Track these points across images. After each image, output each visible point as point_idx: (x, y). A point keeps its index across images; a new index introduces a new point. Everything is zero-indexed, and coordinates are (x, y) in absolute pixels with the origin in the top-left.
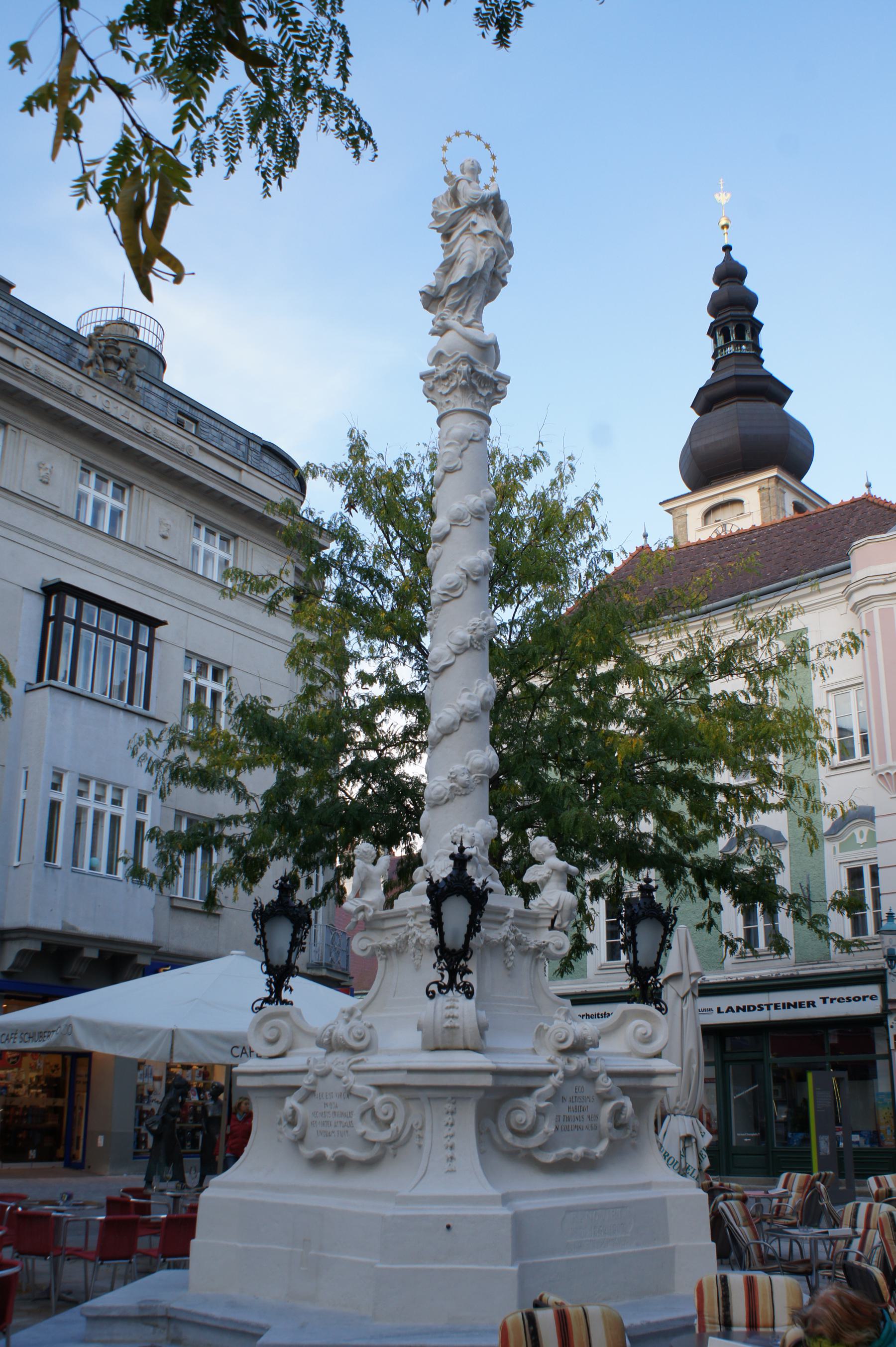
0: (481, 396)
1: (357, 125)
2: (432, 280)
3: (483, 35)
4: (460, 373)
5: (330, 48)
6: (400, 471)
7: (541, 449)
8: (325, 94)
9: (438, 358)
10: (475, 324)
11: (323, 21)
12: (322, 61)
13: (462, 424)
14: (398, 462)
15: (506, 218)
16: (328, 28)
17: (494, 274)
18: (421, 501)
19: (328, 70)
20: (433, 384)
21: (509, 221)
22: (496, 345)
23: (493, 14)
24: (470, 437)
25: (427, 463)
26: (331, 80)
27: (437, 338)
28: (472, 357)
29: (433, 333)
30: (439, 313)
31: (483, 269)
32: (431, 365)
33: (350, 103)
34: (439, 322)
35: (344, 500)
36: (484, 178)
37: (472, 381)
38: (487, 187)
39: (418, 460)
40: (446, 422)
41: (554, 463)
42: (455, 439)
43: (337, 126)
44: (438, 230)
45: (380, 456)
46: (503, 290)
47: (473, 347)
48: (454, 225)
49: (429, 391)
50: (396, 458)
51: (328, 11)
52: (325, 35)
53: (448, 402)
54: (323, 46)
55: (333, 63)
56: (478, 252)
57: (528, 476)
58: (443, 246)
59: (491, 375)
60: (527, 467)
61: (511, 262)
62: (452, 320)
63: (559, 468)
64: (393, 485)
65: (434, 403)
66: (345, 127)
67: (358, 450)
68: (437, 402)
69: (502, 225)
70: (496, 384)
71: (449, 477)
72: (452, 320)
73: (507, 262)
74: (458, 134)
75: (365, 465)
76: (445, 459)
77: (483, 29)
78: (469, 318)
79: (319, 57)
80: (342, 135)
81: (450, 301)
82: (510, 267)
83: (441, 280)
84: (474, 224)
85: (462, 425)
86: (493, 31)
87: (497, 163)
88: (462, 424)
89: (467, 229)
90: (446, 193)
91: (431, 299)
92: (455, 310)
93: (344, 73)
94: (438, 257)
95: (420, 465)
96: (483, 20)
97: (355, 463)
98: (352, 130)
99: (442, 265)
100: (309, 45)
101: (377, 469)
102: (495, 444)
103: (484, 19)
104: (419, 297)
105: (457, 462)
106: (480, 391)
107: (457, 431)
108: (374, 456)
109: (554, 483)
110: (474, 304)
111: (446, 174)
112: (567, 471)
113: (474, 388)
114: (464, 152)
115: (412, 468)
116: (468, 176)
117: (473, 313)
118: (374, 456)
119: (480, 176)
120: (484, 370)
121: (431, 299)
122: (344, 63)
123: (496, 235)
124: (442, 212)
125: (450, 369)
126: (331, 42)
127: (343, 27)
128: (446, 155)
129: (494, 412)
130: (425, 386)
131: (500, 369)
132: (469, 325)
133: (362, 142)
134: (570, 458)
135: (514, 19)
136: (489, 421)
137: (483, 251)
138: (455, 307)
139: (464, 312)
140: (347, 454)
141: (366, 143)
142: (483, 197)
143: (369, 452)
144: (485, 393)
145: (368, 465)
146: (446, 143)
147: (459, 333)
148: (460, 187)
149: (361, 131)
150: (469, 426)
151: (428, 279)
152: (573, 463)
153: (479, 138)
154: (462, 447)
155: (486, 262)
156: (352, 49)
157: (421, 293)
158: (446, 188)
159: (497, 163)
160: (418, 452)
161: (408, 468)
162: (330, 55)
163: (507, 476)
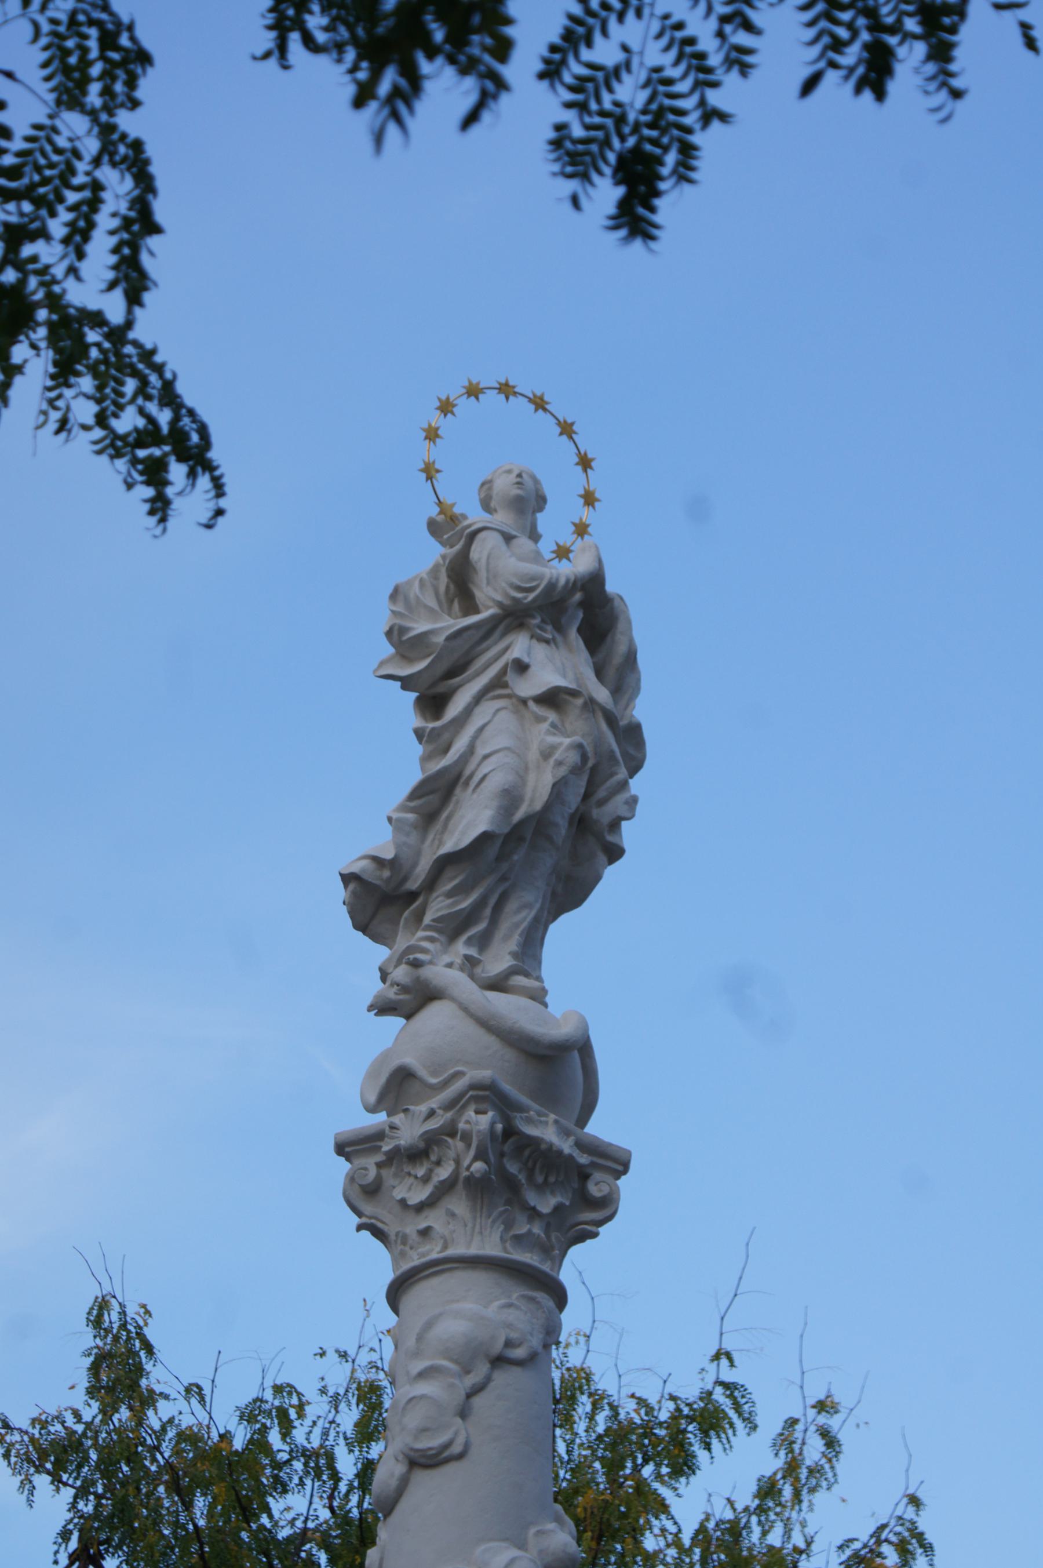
0: (533, 1213)
1: (164, 417)
2: (381, 840)
3: (575, 201)
4: (466, 1138)
5: (94, 204)
6: (259, 1443)
7: (728, 1375)
8: (69, 330)
9: (397, 1086)
10: (519, 980)
11: (74, 125)
12: (66, 241)
13: (469, 1306)
14: (249, 1414)
15: (622, 649)
16: (91, 146)
17: (582, 823)
18: (325, 1544)
19: (84, 267)
20: (378, 1171)
21: (631, 659)
22: (584, 1048)
23: (606, 143)
24: (498, 1347)
25: (349, 1417)
26: (90, 289)
27: (396, 1023)
28: (507, 1087)
29: (383, 1008)
30: (402, 942)
31: (548, 807)
32: (372, 1110)
33: (147, 355)
34: (401, 973)
35: (65, 1535)
36: (555, 526)
37: (507, 1163)
38: (562, 553)
39: (318, 1407)
40: (412, 1299)
41: (770, 1425)
42: (446, 1354)
43: (101, 420)
44: (407, 683)
45: (194, 1391)
46: (612, 874)
47: (510, 1055)
48: (457, 670)
49: (363, 1194)
50: (245, 1398)
51: (94, 96)
52: (81, 167)
53: (425, 1233)
54: (72, 197)
55: (101, 249)
56: (533, 755)
57: (683, 1465)
58: (419, 734)
59: (566, 1147)
60: (681, 1436)
61: (637, 785)
62: (444, 968)
63: (786, 1439)
64: (234, 1489)
65: (379, 1234)
66: (127, 422)
67: (120, 1366)
68: (391, 1230)
69: (611, 672)
70: (584, 1176)
71: (424, 1482)
72: (444, 968)
73: (624, 785)
74: (473, 391)
75: (140, 1420)
76: (414, 1419)
77: (572, 186)
78: (498, 960)
79: (57, 228)
80: (116, 446)
81: (438, 907)
82: (633, 801)
83: (413, 839)
84: (521, 667)
85: (470, 1309)
86: (606, 194)
87: (597, 480)
88: (469, 1306)
89: (498, 683)
90: (435, 571)
91: (379, 900)
92: (453, 937)
93: (132, 279)
94: (404, 768)
95: (326, 1422)
96: (574, 157)
97: (107, 1412)
98: (150, 435)
99: (416, 793)
100: (27, 193)
101: (182, 1437)
102: (575, 1358)
103: (571, 155)
104: (339, 892)
105: (450, 1433)
106: (532, 1198)
107: (453, 1328)
108: (175, 1389)
109: (768, 1490)
110: (516, 917)
111: (434, 511)
112: (813, 1450)
113: (512, 1186)
114: (490, 447)
115: (299, 1435)
116: (503, 519)
117: (513, 944)
118: (175, 1389)
119: (543, 520)
120: (547, 1131)
121: (379, 900)
122: (135, 249)
123: (591, 704)
124: (420, 627)
125: (433, 1124)
126: (97, 187)
127: (137, 146)
128: (438, 454)
129: (579, 1266)
130: (351, 1179)
131: (600, 1127)
132: (498, 985)
133: (177, 471)
134: (821, 1406)
135: (671, 158)
136: (560, 1298)
137: (546, 754)
138: (453, 928)
139: (483, 941)
140: (83, 1382)
141: (192, 475)
142: (551, 586)
143: (157, 1376)
144: (546, 1205)
145: (154, 1421)
146: (436, 419)
147: (465, 1009)
148: (478, 553)
149: (177, 438)
150: (492, 1311)
151: (370, 833)
152: (834, 1422)
153: (539, 404)
154: (470, 1380)
155: (558, 789)
156: (161, 210)
157: (347, 879)
158: (432, 553)
159: (597, 480)
160: (315, 1377)
161: (286, 1432)
162: (91, 225)
163: (613, 1467)
